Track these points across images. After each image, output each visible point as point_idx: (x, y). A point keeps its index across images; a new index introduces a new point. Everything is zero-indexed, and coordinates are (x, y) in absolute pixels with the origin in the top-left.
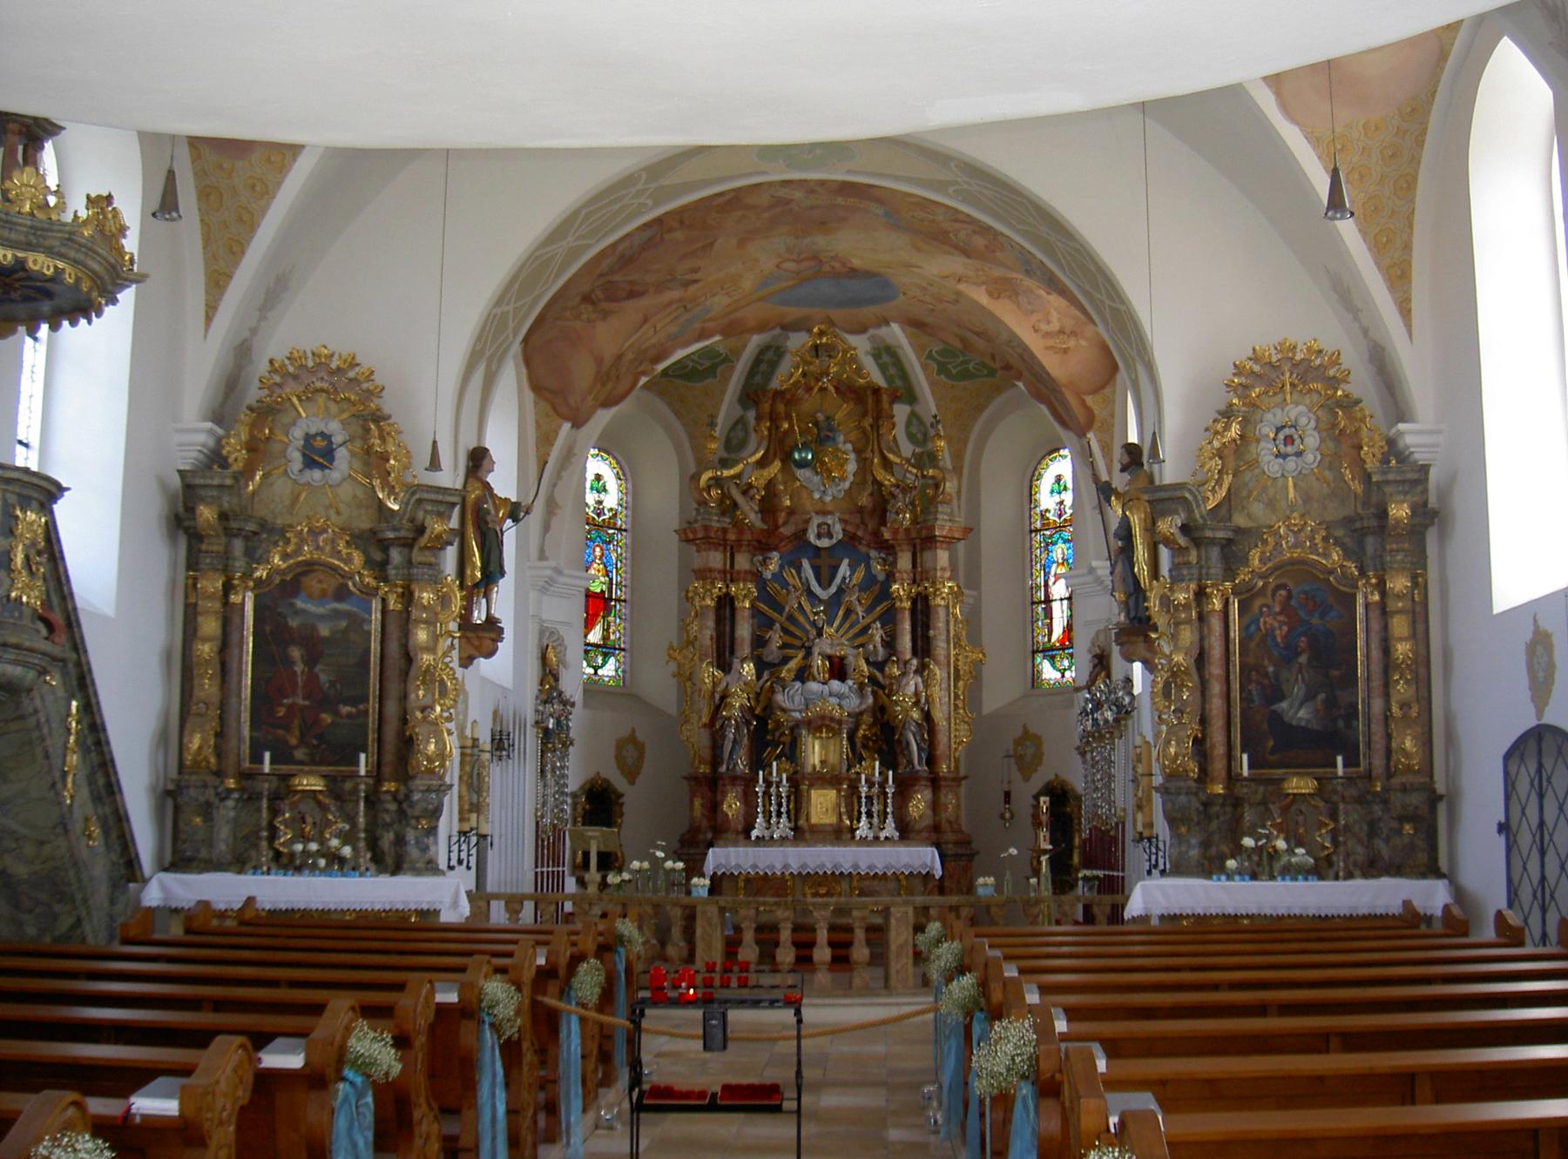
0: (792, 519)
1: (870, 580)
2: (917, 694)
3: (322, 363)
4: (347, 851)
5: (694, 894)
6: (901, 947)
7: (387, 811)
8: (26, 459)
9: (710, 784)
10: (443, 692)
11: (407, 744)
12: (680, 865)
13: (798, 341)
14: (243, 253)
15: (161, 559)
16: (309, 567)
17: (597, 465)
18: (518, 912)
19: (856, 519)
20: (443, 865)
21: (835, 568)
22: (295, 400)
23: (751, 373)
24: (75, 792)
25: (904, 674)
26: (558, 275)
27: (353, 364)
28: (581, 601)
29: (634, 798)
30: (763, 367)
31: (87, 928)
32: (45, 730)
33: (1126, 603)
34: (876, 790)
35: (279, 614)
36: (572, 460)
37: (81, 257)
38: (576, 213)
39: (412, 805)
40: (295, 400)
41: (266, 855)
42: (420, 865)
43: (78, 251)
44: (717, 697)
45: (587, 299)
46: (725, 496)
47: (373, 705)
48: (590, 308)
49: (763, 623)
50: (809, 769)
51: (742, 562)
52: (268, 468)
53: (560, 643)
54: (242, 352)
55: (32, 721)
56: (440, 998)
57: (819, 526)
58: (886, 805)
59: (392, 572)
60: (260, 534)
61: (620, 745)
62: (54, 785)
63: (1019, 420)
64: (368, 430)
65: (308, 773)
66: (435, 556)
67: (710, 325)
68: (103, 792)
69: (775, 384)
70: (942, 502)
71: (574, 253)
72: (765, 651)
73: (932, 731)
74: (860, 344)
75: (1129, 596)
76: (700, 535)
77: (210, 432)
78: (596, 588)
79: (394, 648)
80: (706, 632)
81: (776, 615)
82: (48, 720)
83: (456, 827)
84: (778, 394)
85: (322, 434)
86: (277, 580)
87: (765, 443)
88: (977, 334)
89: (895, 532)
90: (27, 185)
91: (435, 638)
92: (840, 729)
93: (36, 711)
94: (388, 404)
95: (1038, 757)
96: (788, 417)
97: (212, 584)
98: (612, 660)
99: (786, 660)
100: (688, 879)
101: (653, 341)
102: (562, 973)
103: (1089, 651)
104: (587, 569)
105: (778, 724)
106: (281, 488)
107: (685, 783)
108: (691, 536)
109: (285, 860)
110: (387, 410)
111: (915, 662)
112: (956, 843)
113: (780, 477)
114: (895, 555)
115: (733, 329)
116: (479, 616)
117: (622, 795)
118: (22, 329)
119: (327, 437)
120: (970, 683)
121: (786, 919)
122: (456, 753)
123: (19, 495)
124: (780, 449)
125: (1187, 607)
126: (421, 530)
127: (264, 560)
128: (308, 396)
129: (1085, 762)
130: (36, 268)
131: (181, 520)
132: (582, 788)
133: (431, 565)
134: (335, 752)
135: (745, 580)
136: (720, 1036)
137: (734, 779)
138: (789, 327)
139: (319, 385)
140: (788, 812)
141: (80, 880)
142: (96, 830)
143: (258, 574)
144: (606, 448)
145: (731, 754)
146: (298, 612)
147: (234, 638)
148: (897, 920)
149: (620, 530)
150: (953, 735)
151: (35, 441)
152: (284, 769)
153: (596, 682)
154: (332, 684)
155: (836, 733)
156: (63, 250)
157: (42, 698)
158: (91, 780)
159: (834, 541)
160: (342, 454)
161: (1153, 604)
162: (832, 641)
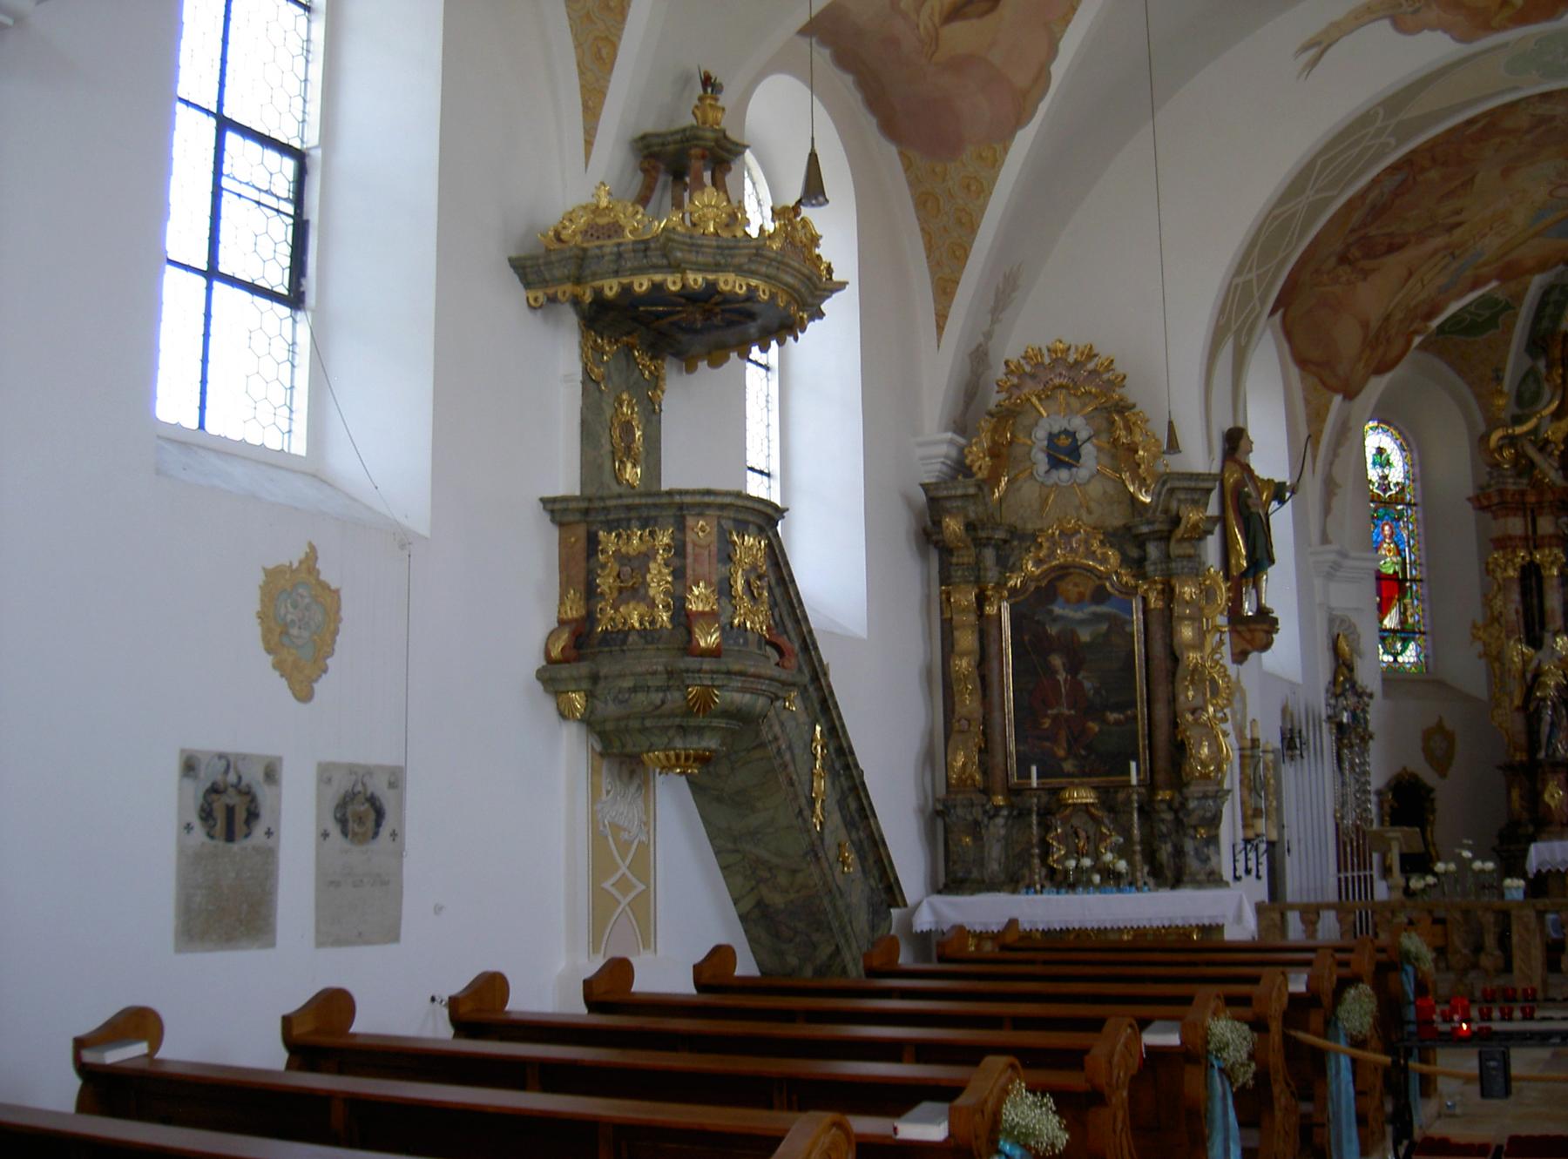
3: (1058, 357)
4: (1122, 865)
5: (1508, 896)
7: (1163, 821)
8: (756, 487)
10: (1215, 691)
11: (1179, 750)
12: (1490, 865)
14: (967, 257)
15: (912, 576)
16: (1064, 571)
17: (1376, 439)
18: (1314, 923)
20: (1227, 874)
22: (1034, 399)
23: (1538, 317)
24: (825, 817)
26: (1301, 235)
27: (1091, 356)
28: (1371, 585)
29: (1447, 794)
30: (1549, 310)
31: (847, 956)
32: (788, 757)
35: (1038, 622)
36: (1349, 437)
37: (772, 271)
38: (1310, 165)
39: (1189, 813)
40: (1034, 399)
41: (1039, 873)
42: (1202, 877)
43: (769, 266)
44: (1529, 676)
45: (1343, 259)
46: (1520, 455)
47: (1141, 710)
51: (1546, 525)
52: (1012, 474)
53: (1352, 631)
54: (979, 357)
55: (772, 749)
56: (1151, 1038)
59: (1150, 568)
60: (1011, 542)
61: (1427, 736)
62: (801, 811)
65: (1082, 785)
66: (1193, 546)
67: (1485, 270)
68: (857, 817)
71: (1315, 210)
76: (1495, 500)
77: (951, 442)
78: (1389, 566)
79: (1158, 649)
82: (790, 747)
83: (1240, 834)
85: (1066, 432)
87: (1559, 392)
90: (709, 206)
91: (1202, 635)
93: (776, 739)
94: (1132, 392)
97: (966, 597)
98: (1412, 646)
100: (1501, 880)
102: (1327, 1000)
104: (1377, 549)
106: (1031, 491)
108: (1485, 503)
109: (1059, 877)
110: (1131, 400)
115: (1511, 272)
116: (1248, 609)
117: (1432, 790)
118: (734, 356)
119: (1072, 435)
122: (1235, 756)
123: (735, 520)
126: (1176, 521)
127: (1016, 568)
128: (1047, 395)
130: (728, 288)
131: (929, 536)
132: (1388, 784)
133: (1190, 557)
134: (1104, 764)
135: (1550, 546)
136: (1501, 1080)
139: (1057, 381)
141: (835, 907)
142: (851, 856)
143: (1012, 583)
144: (1385, 419)
145: (1549, 737)
146: (1056, 619)
147: (993, 649)
149: (1409, 505)
151: (775, 468)
152: (1054, 782)
153: (1395, 670)
154: (1097, 691)
156: (753, 267)
157: (782, 724)
158: (842, 804)
160: (1088, 451)
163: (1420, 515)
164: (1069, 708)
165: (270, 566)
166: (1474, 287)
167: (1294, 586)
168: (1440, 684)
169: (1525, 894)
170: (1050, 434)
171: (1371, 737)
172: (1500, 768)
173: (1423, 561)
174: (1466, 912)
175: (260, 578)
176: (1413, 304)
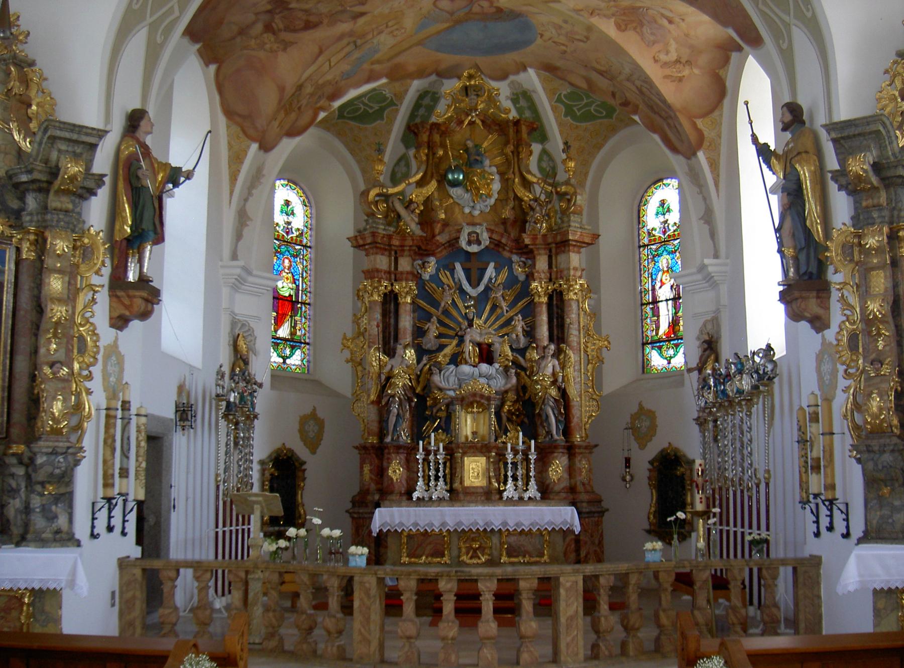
0: (447, 230)
1: (512, 280)
2: (554, 374)
5: (352, 563)
6: (571, 618)
7: (13, 475)
9: (377, 452)
12: (337, 533)
13: (452, 86)
17: (283, 193)
19: (501, 229)
21: (484, 270)
25: (543, 358)
33: (796, 259)
34: (520, 457)
42: (47, 535)
44: (383, 377)
46: (391, 209)
49: (422, 316)
50: (463, 440)
51: (405, 264)
53: (250, 333)
57: (469, 234)
58: (528, 470)
61: (304, 421)
63: (641, 144)
64: (8, 73)
66: (73, 202)
67: (377, 67)
69: (434, 119)
70: (574, 213)
72: (424, 340)
73: (567, 406)
74: (503, 90)
75: (798, 250)
76: (369, 240)
78: (285, 288)
80: (373, 323)
81: (433, 310)
84: (436, 126)
87: (424, 167)
88: (601, 73)
89: (534, 238)
92: (489, 405)
94: (29, 50)
95: (653, 428)
96: (443, 146)
98: (298, 352)
99: (442, 347)
101: (329, 77)
103: (698, 338)
105: (436, 401)
107: (357, 451)
108: (361, 242)
110: (31, 56)
111: (552, 347)
112: (589, 502)
113: (436, 195)
114: (534, 259)
115: (397, 74)
120: (596, 363)
121: (450, 591)
124: (437, 172)
125: (879, 250)
126: (54, 172)
129: (702, 432)
132: (270, 456)
135: (407, 280)
137: (398, 448)
138: (443, 74)
140: (445, 476)
145: (395, 426)
148: (567, 590)
149: (305, 246)
150: (583, 411)
155: (486, 408)
159: (482, 247)
161: (834, 252)
162: (481, 331)
166: (368, 80)
168: (317, 383)
169: (368, 563)
171: (256, 417)
172: (356, 448)
174: (314, 576)
176: (320, 82)
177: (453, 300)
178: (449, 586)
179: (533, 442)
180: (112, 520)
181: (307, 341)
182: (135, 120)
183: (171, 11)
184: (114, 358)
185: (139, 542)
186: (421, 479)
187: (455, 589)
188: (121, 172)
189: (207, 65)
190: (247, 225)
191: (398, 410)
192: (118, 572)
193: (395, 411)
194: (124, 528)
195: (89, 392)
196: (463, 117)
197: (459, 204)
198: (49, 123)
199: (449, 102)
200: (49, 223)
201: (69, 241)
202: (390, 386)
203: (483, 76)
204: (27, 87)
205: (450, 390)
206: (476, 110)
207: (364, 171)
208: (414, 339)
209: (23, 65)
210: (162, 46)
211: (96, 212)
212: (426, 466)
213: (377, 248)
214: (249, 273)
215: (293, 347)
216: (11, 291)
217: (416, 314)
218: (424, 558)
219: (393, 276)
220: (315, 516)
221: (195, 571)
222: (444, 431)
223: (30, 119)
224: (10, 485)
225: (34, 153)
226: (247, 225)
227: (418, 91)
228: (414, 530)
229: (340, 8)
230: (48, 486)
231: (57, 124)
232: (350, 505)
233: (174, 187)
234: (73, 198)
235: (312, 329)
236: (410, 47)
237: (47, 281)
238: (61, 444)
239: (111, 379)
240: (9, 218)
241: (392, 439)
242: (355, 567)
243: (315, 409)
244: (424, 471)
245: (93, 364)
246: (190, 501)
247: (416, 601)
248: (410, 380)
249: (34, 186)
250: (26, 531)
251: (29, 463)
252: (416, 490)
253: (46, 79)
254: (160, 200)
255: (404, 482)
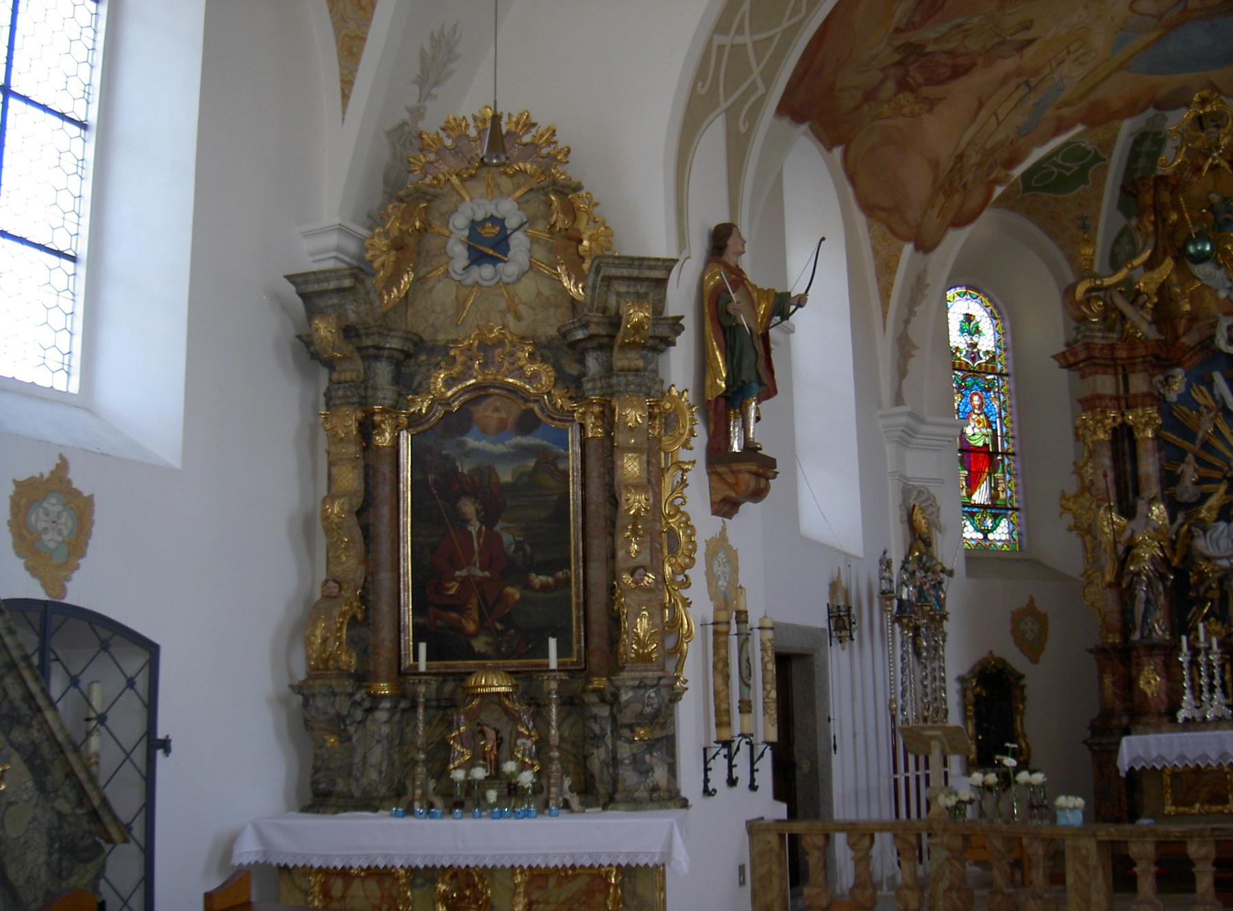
4: (526, 778)
7: (595, 717)
9: (1120, 657)
13: (1179, 118)
15: (281, 405)
17: (960, 306)
35: (447, 457)
40: (454, 179)
42: (642, 794)
44: (1121, 548)
46: (1110, 308)
48: (910, 97)
49: (1171, 455)
51: (1138, 383)
52: (423, 271)
60: (413, 358)
61: (1017, 618)
64: (549, 204)
65: (495, 670)
66: (644, 357)
67: (1066, 112)
69: (1160, 171)
72: (1178, 489)
76: (1082, 356)
78: (976, 434)
81: (1186, 445)
84: (1163, 179)
85: (493, 219)
86: (440, 411)
87: (1151, 241)
94: (571, 172)
96: (1176, 207)
98: (1004, 523)
99: (1205, 497)
105: (1202, 576)
108: (1072, 360)
110: (575, 179)
113: (1174, 279)
115: (1098, 116)
117: (1022, 677)
119: (498, 221)
124: (1172, 245)
126: (615, 322)
132: (972, 670)
134: (518, 642)
135: (1144, 406)
137: (1152, 648)
138: (1165, 104)
140: (1223, 685)
146: (469, 453)
147: (384, 491)
149: (1000, 375)
151: (82, 249)
154: (519, 546)
160: (519, 242)
163: (1012, 387)
164: (482, 569)
165: (21, 478)
166: (1058, 131)
167: (855, 447)
170: (473, 221)
172: (1091, 651)
173: (1016, 434)
175: (10, 489)
176: (989, 145)
177: (1215, 426)
178: (1203, 851)
179: (1184, 638)
180: (734, 770)
181: (1015, 505)
182: (721, 240)
183: (753, 88)
184: (721, 555)
185: (778, 795)
186: (1187, 692)
187: (1213, 856)
188: (706, 310)
189: (829, 149)
190: (912, 356)
191: (1146, 592)
192: (747, 838)
193: (1143, 595)
194: (753, 780)
195: (687, 603)
196: (1200, 161)
197: (1209, 287)
198: (600, 261)
199: (1178, 143)
200: (615, 389)
201: (643, 408)
202: (1132, 561)
203: (1222, 97)
204: (575, 219)
205: (1221, 558)
206: (1218, 148)
207: (1072, 260)
208: (1163, 490)
209: (566, 191)
210: (748, 134)
211: (678, 367)
212: (1195, 673)
213: (1095, 365)
214: (922, 421)
215: (995, 517)
216: (579, 480)
217: (1163, 454)
218: (1197, 806)
219: (1123, 403)
220: (1006, 754)
221: (849, 835)
222: (1218, 618)
223: (582, 259)
224: (592, 731)
225: (588, 301)
226: (912, 356)
227: (1132, 134)
228: (1180, 766)
229: (996, 40)
230: (637, 729)
231: (611, 260)
232: (1088, 734)
233: (782, 320)
234: (644, 352)
235: (1020, 488)
236: (1109, 75)
237: (619, 463)
238: (650, 674)
239: (720, 583)
240: (567, 388)
241: (1142, 636)
242: (1066, 827)
243: (1032, 601)
244: (1192, 679)
245: (689, 566)
246: (860, 738)
247: (1216, 872)
248: (1161, 548)
249: (594, 344)
250: (615, 790)
251: (613, 700)
252: (1181, 707)
253: (596, 205)
254: (765, 338)
255: (1164, 697)
